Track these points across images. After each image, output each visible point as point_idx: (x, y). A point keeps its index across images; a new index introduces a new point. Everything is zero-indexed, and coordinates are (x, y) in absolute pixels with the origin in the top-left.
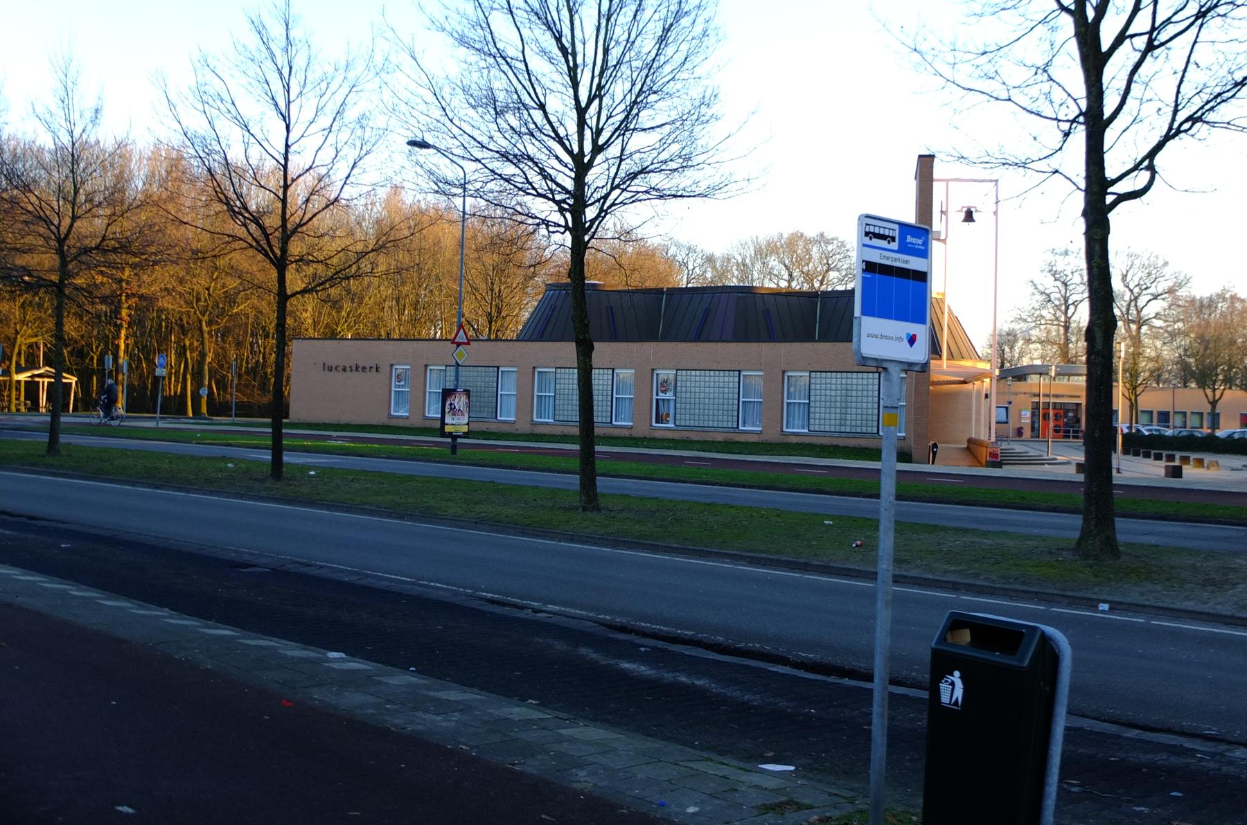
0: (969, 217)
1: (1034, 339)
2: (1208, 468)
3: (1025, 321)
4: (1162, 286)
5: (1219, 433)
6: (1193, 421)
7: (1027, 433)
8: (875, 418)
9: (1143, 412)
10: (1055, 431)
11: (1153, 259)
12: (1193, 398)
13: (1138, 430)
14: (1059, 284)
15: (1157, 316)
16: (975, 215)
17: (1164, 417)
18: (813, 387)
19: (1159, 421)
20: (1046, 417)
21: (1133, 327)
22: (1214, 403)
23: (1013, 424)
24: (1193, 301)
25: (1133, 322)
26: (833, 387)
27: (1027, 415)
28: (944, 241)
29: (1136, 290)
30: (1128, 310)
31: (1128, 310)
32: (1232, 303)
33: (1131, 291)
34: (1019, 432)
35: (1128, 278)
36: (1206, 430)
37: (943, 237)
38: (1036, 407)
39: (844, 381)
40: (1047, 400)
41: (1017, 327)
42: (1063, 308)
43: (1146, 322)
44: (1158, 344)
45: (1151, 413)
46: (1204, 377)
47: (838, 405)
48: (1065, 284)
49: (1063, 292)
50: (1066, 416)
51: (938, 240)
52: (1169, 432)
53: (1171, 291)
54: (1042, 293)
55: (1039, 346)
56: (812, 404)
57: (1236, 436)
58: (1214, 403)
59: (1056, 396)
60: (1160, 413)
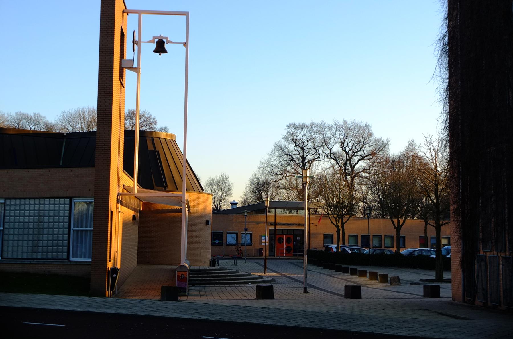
0: (160, 47)
1: (281, 186)
2: (391, 284)
3: (276, 174)
4: (367, 150)
5: (403, 252)
7: (266, 253)
8: (66, 243)
9: (374, 236)
10: (287, 251)
12: (383, 226)
13: (344, 250)
14: (299, 149)
15: (364, 170)
16: (167, 46)
17: (366, 240)
18: (7, 213)
19: (362, 243)
20: (280, 240)
21: (349, 178)
22: (398, 228)
23: (255, 246)
24: (387, 160)
25: (349, 175)
26: (27, 213)
27: (265, 239)
28: (136, 70)
29: (350, 153)
30: (345, 166)
32: (413, 160)
33: (347, 153)
34: (260, 252)
35: (346, 144)
36: (394, 250)
37: (135, 66)
38: (272, 233)
39: (37, 207)
40: (272, 227)
41: (270, 178)
42: (301, 165)
43: (357, 175)
44: (364, 188)
45: (356, 237)
46: (395, 214)
47: (31, 231)
48: (303, 148)
49: (301, 154)
50: (295, 240)
51: (131, 68)
52: (366, 251)
53: (373, 154)
54: (287, 155)
55: (284, 191)
56: (6, 231)
57: (416, 254)
58: (398, 228)
59: (279, 224)
60: (362, 237)
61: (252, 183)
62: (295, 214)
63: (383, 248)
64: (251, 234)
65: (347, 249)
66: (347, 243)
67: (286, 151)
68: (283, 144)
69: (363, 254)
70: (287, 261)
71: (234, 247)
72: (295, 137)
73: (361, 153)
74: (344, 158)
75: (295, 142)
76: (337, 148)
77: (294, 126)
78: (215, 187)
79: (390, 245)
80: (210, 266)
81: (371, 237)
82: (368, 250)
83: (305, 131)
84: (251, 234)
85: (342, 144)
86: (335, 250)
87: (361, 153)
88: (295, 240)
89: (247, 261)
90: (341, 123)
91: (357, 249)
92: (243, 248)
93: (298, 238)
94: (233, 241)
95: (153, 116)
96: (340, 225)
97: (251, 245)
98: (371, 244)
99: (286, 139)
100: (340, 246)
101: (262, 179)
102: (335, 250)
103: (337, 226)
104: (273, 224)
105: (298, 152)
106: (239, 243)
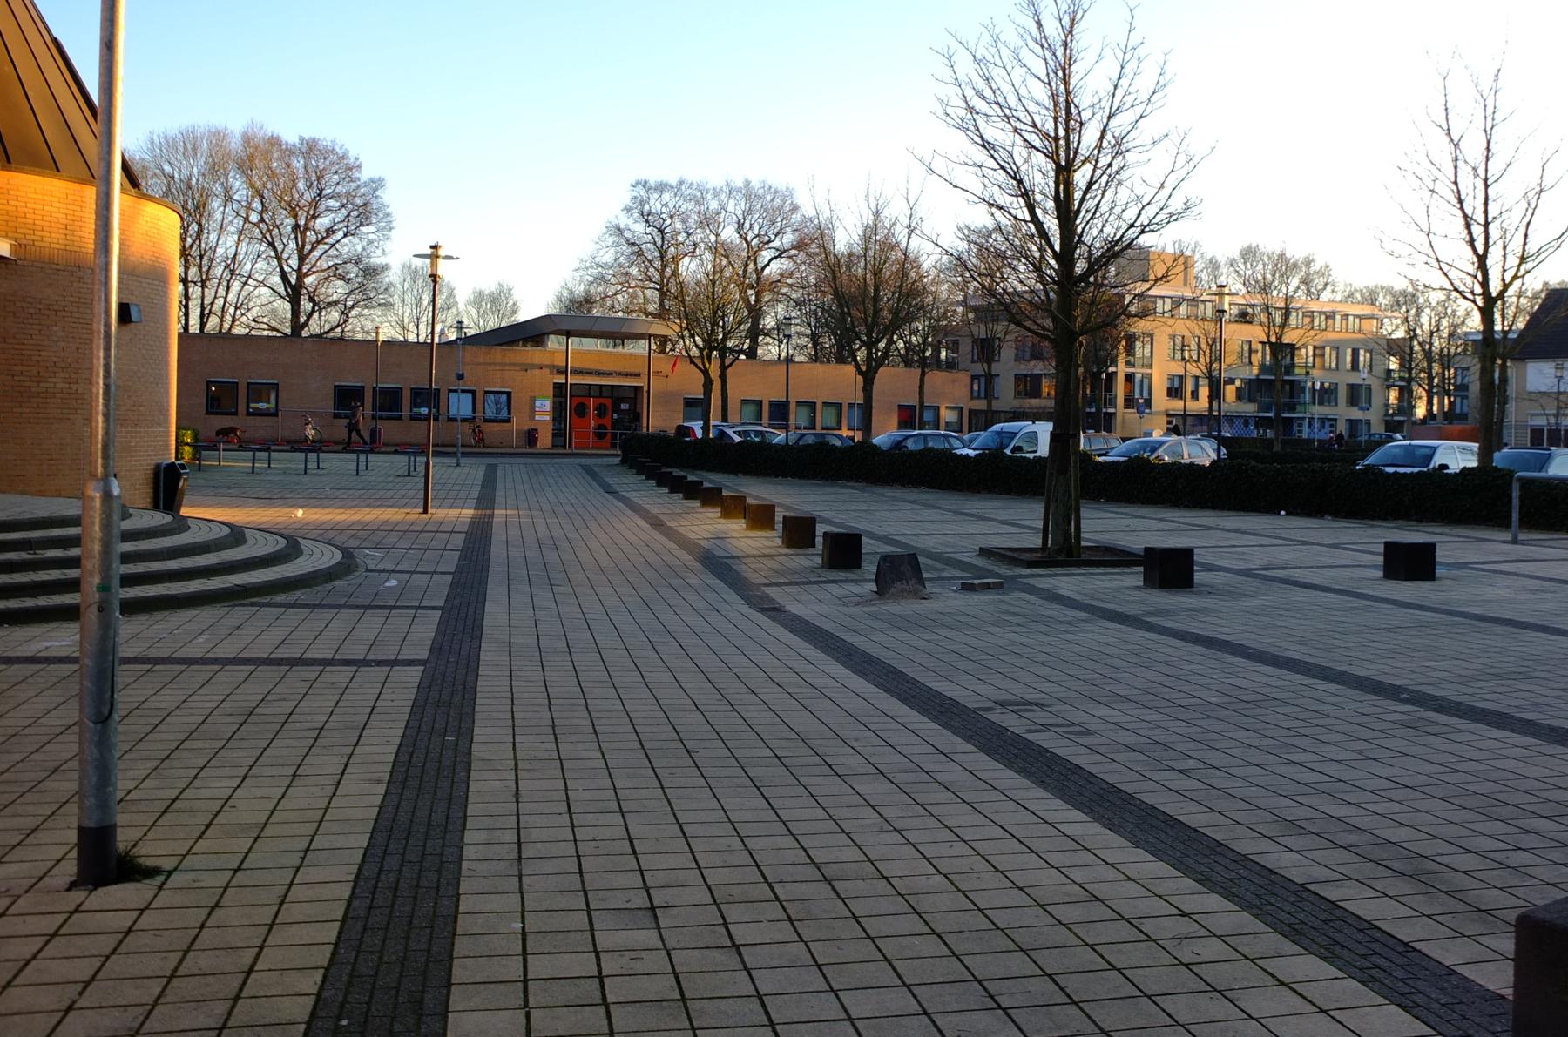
6: (824, 418)
10: (600, 436)
11: (778, 202)
13: (722, 434)
17: (780, 412)
20: (581, 411)
23: (519, 423)
25: (752, 287)
27: (545, 405)
30: (745, 271)
31: (745, 271)
34: (531, 437)
35: (747, 225)
38: (559, 389)
48: (661, 231)
50: (616, 409)
52: (779, 437)
59: (576, 372)
61: (559, 299)
62: (619, 349)
63: (819, 430)
64: (509, 394)
65: (730, 432)
66: (734, 418)
67: (627, 234)
68: (624, 221)
69: (770, 445)
70: (577, 460)
71: (466, 425)
72: (647, 207)
73: (776, 243)
74: (744, 254)
75: (646, 217)
76: (729, 233)
77: (645, 184)
78: (486, 306)
79: (834, 424)
80: (156, 507)
81: (792, 406)
82: (783, 435)
83: (666, 197)
84: (509, 394)
85: (740, 226)
86: (699, 434)
87: (776, 243)
88: (616, 409)
89: (463, 461)
90: (740, 184)
91: (757, 433)
92: (487, 427)
93: (624, 406)
94: (466, 411)
95: (352, 155)
96: (714, 370)
97: (509, 421)
98: (792, 421)
99: (628, 209)
100: (712, 423)
101: (579, 290)
102: (699, 434)
103: (705, 372)
104: (563, 371)
105: (655, 251)
106: (479, 414)
